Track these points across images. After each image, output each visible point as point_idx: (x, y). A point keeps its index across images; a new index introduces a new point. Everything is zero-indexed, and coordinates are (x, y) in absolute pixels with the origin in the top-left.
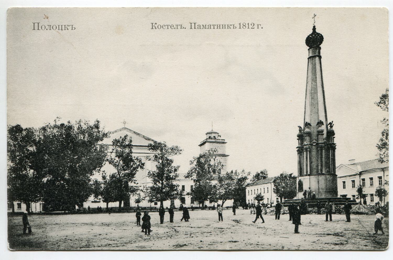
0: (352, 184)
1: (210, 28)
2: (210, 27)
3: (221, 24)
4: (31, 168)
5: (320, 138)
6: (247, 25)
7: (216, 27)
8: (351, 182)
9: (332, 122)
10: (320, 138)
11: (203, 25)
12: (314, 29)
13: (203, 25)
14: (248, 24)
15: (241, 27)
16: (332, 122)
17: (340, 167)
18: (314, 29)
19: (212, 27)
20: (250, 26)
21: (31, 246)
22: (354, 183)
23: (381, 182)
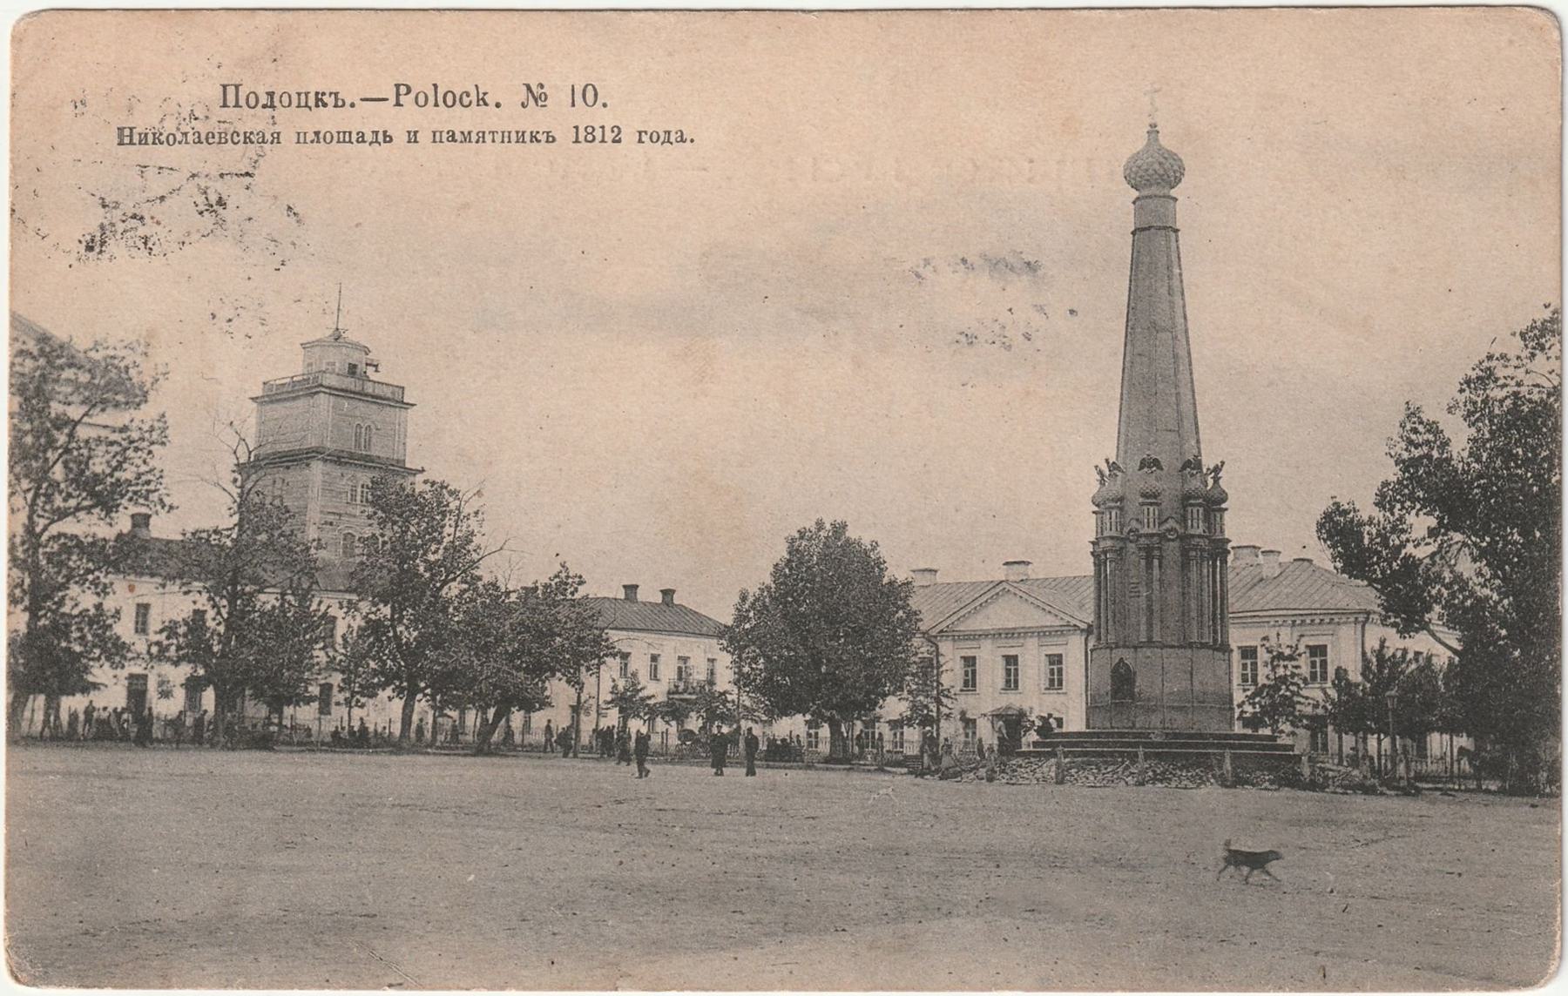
0: (1004, 673)
1: (484, 142)
2: (483, 137)
3: (151, 146)
4: (1501, 628)
5: (1189, 517)
6: (598, 133)
7: (498, 137)
8: (1001, 663)
9: (1223, 463)
10: (1189, 517)
11: (462, 133)
12: (1153, 130)
13: (462, 133)
14: (603, 127)
15: (581, 138)
16: (1223, 463)
17: (997, 594)
18: (1153, 130)
19: (488, 138)
20: (609, 136)
21: (446, 488)
22: (1012, 668)
23: (370, 399)
